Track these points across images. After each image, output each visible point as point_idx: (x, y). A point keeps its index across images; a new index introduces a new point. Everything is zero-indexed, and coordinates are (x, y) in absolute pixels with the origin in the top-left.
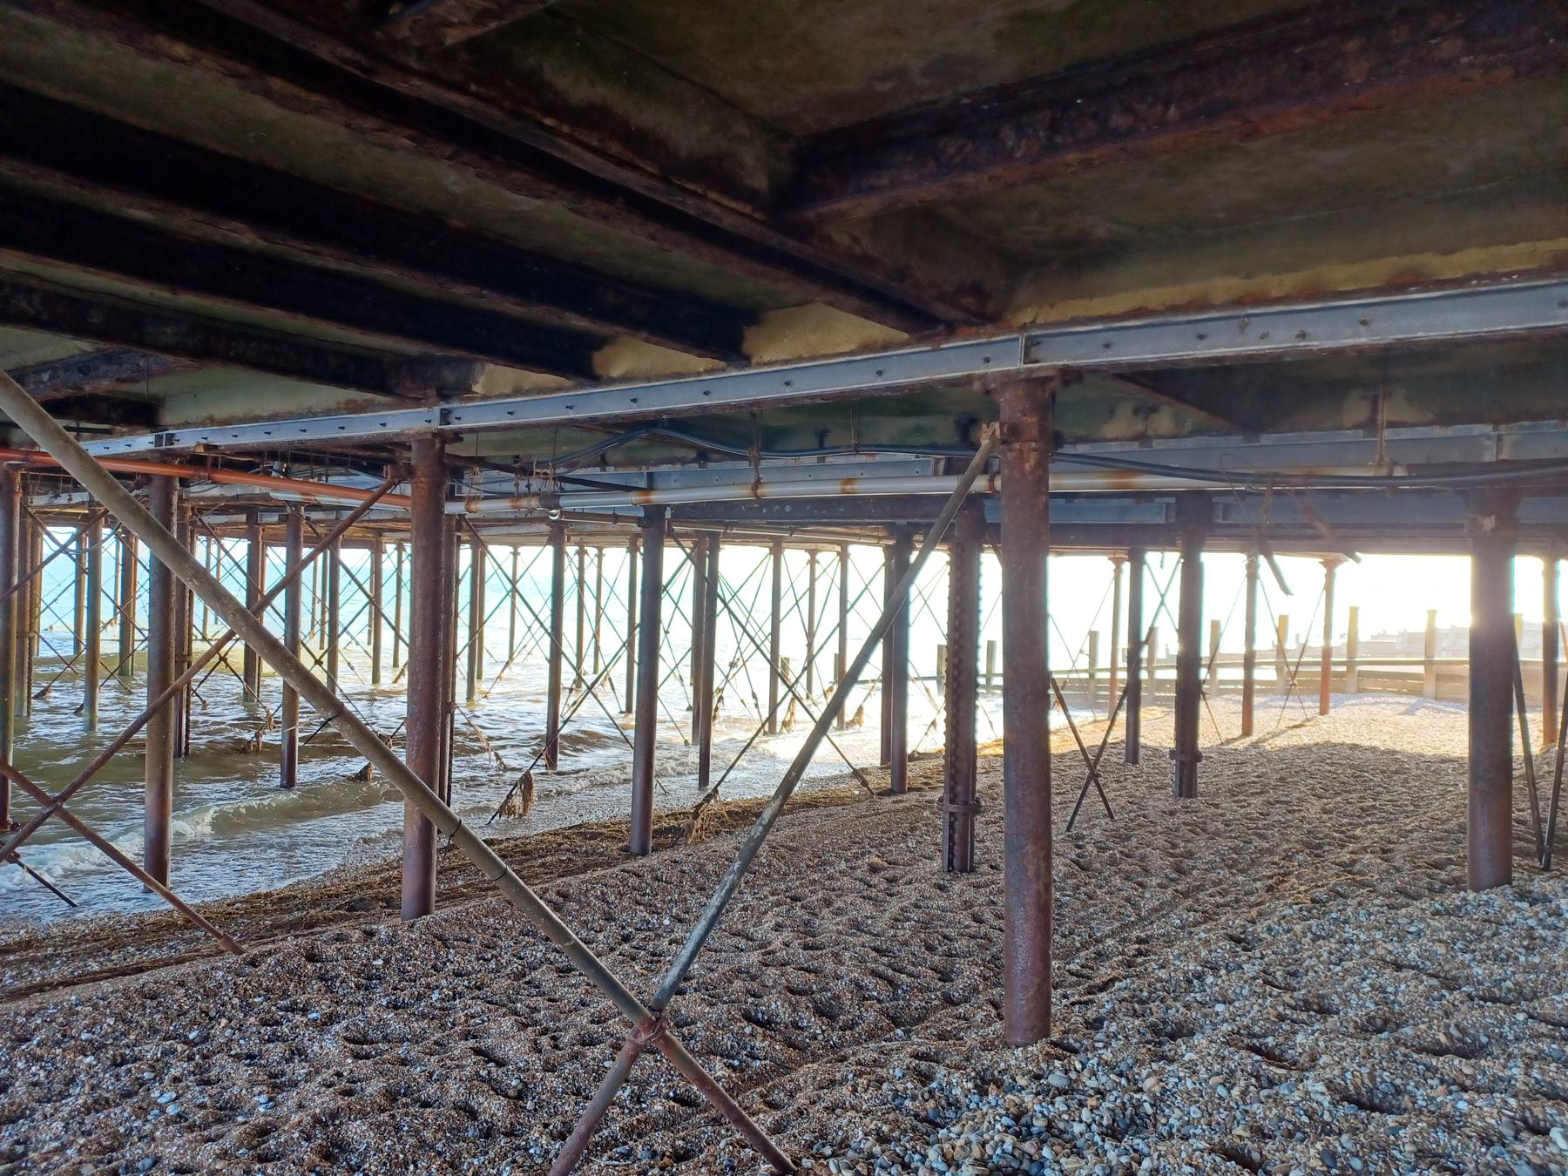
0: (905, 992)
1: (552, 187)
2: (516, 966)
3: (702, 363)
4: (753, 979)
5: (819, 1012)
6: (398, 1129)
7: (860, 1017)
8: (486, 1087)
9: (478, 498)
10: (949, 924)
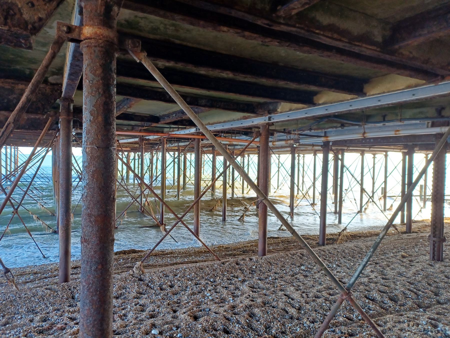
0: (421, 297)
1: (315, 50)
2: (291, 273)
3: (348, 96)
4: (366, 286)
5: (391, 299)
6: (267, 313)
7: (406, 303)
8: (289, 305)
9: (276, 141)
10: (436, 277)
